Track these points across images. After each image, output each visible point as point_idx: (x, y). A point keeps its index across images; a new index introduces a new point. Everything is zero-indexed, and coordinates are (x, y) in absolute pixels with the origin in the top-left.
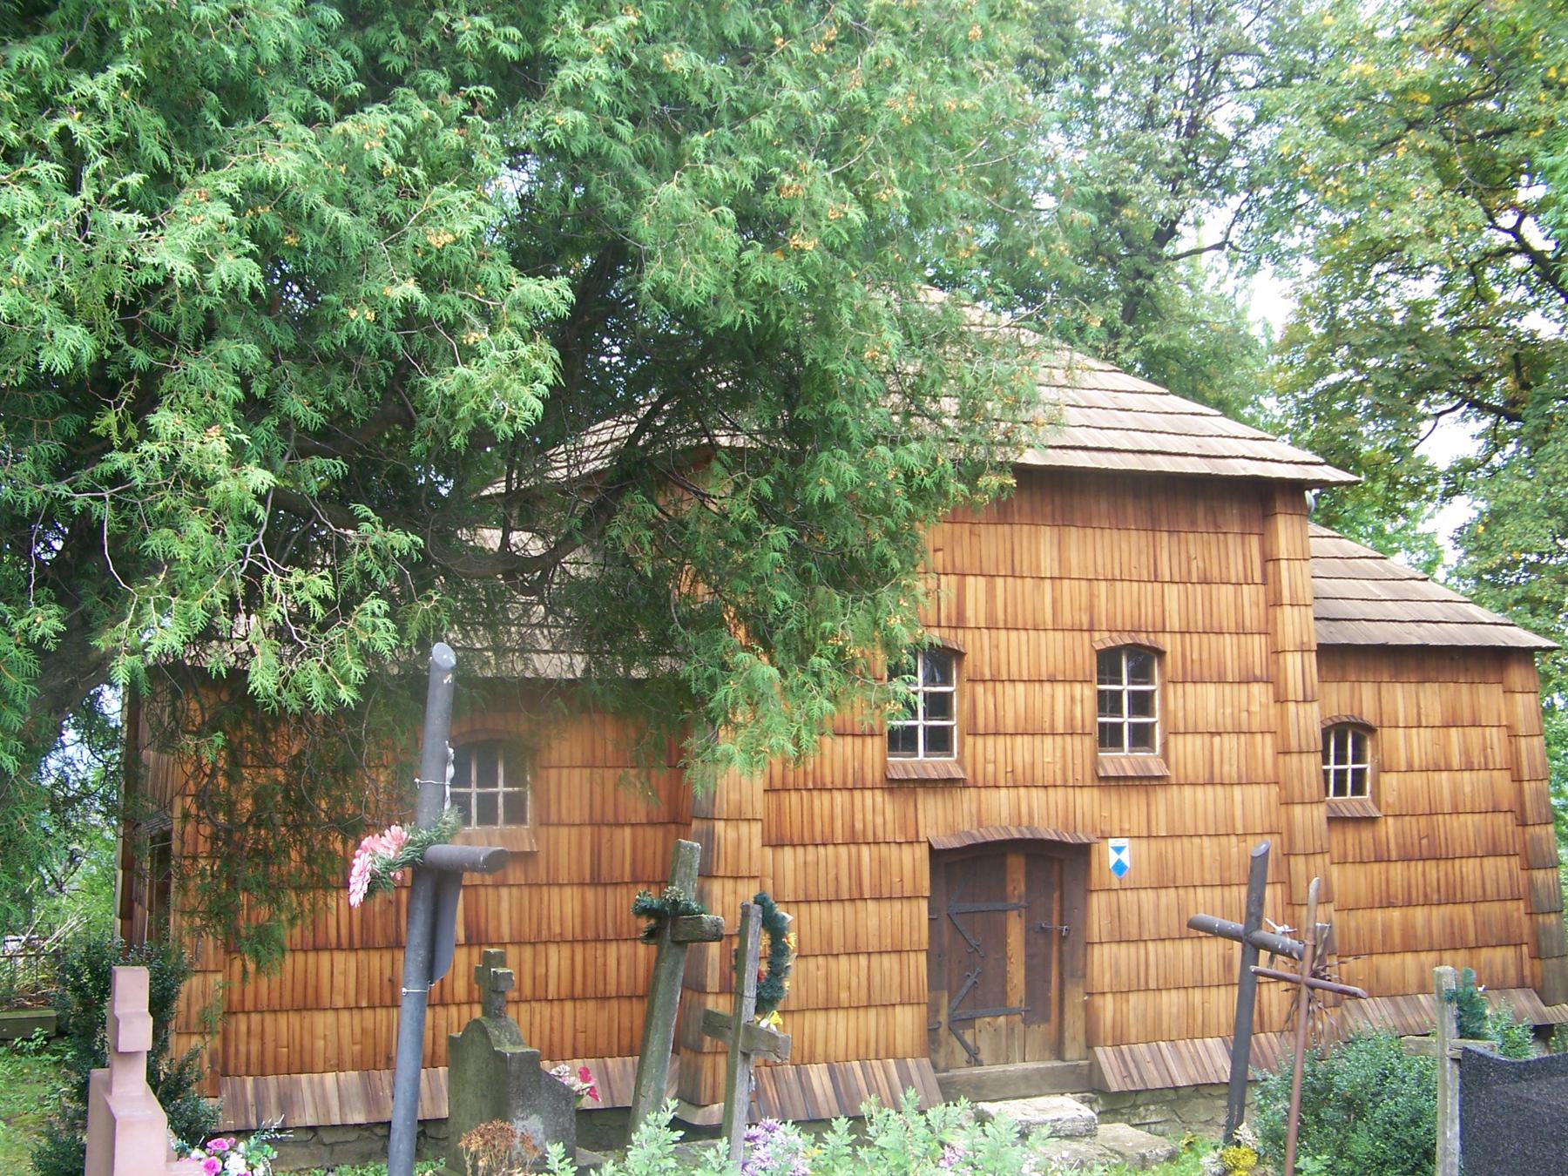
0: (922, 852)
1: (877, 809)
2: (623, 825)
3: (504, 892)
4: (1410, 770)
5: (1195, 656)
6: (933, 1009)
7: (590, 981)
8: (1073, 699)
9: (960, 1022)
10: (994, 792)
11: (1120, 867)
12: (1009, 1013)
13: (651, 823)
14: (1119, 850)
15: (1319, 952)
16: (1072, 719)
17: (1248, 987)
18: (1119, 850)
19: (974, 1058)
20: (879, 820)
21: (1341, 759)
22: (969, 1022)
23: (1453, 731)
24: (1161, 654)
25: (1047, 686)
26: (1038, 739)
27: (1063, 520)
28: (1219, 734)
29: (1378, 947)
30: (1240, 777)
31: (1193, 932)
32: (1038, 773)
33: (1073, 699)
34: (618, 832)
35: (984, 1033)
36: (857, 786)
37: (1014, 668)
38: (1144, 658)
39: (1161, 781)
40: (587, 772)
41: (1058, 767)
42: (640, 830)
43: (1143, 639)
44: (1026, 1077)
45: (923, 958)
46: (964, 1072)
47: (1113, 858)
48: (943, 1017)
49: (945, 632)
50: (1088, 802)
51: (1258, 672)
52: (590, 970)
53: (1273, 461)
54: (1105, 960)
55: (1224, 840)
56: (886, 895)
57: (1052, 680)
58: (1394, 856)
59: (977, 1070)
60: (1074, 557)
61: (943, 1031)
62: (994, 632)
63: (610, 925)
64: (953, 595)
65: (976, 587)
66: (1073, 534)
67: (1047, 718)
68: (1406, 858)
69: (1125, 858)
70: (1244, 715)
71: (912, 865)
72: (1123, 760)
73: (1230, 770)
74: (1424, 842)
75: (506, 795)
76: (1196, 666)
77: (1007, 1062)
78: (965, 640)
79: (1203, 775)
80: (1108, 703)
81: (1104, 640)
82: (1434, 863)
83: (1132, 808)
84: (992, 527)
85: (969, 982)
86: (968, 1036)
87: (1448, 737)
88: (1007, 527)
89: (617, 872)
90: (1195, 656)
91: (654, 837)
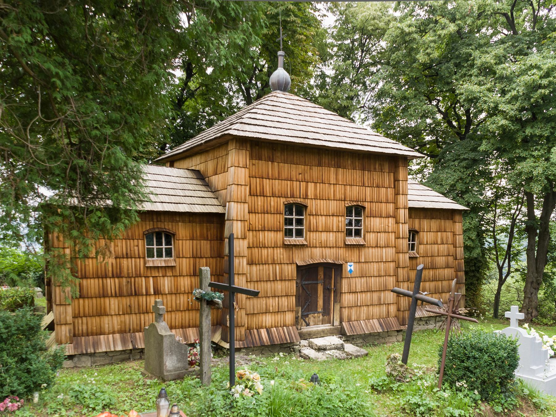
1: (280, 254)
3: (166, 278)
4: (427, 244)
5: (374, 209)
11: (351, 271)
12: (319, 313)
13: (211, 257)
14: (351, 266)
16: (339, 227)
18: (351, 266)
20: (282, 257)
26: (328, 233)
34: (201, 260)
40: (191, 241)
42: (208, 259)
45: (294, 298)
47: (349, 268)
48: (300, 314)
49: (302, 200)
50: (342, 252)
54: (347, 299)
55: (380, 263)
57: (333, 215)
60: (340, 177)
69: (352, 268)
71: (290, 270)
73: (382, 243)
75: (165, 248)
78: (308, 203)
81: (348, 204)
85: (307, 304)
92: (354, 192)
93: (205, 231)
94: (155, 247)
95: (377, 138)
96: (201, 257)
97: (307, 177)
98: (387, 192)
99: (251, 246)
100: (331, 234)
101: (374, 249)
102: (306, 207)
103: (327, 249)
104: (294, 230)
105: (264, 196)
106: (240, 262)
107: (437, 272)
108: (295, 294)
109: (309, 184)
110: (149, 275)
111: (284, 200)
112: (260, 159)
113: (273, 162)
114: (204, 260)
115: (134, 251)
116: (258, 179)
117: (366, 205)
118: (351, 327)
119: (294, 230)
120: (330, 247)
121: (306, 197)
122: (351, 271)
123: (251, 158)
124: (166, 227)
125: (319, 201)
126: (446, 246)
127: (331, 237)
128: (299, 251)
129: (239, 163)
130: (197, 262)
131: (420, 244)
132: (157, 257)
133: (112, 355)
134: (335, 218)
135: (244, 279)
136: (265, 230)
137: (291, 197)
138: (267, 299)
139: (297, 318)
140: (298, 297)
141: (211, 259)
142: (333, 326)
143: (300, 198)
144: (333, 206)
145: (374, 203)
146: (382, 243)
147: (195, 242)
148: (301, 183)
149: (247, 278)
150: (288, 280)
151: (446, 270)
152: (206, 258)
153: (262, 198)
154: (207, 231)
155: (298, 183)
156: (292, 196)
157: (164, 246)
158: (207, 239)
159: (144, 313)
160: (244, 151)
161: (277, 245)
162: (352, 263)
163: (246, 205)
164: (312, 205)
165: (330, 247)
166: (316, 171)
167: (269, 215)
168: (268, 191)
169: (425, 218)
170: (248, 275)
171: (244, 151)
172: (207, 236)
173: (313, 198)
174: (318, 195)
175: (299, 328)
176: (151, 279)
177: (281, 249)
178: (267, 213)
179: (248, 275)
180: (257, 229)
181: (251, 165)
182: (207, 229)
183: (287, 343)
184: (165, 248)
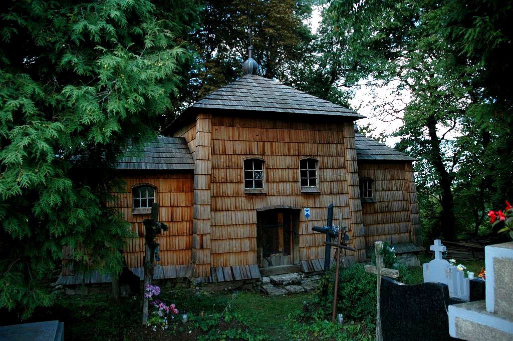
0: (255, 213)
1: (243, 202)
2: (179, 207)
4: (383, 190)
5: (326, 162)
6: (258, 253)
7: (171, 246)
8: (294, 173)
9: (266, 255)
10: (273, 197)
11: (307, 216)
12: (280, 252)
13: (187, 206)
14: (307, 211)
15: (343, 236)
16: (294, 177)
17: (328, 246)
18: (307, 211)
19: (270, 264)
20: (243, 205)
21: (365, 188)
22: (269, 256)
23: (393, 181)
24: (317, 161)
25: (287, 170)
26: (285, 184)
27: (290, 127)
28: (333, 181)
29: (387, 233)
30: (338, 192)
31: (315, 232)
32: (285, 192)
33: (294, 173)
34: (178, 209)
35: (274, 257)
36: (237, 196)
37: (278, 165)
38: (259, 164)
39: (265, 195)
40: (170, 193)
41: (290, 190)
42: (183, 208)
43: (312, 158)
44: (284, 269)
45: (255, 240)
46: (268, 268)
47: (306, 213)
49: (260, 156)
50: (300, 200)
51: (342, 166)
52: (172, 243)
53: (311, 110)
56: (245, 223)
58: (379, 211)
59: (271, 268)
60: (293, 137)
61: (262, 258)
62: (273, 156)
63: (176, 232)
64: (262, 146)
65: (268, 145)
66: (293, 131)
67: (287, 177)
68: (382, 212)
69: (309, 213)
70: (339, 176)
72: (254, 190)
73: (335, 190)
74: (387, 208)
75: (148, 199)
76: (326, 164)
77: (279, 265)
78: (265, 158)
79: (329, 192)
80: (303, 174)
81: (303, 158)
82: (389, 213)
83: (311, 202)
84: (272, 130)
86: (269, 258)
87: (392, 183)
88: (276, 130)
89: (178, 219)
90: (326, 162)
91: (187, 210)
92: (308, 149)
93: (181, 184)
94: (140, 198)
95: (328, 105)
96: (177, 207)
97: (264, 138)
98: (337, 147)
99: (215, 195)
100: (288, 184)
101: (328, 196)
102: (263, 162)
103: (284, 196)
104: (254, 182)
105: (226, 155)
106: (204, 210)
107: (394, 215)
108: (326, 218)
109: (266, 143)
110: (135, 221)
111: (244, 157)
112: (222, 125)
113: (233, 126)
114: (180, 208)
115: (124, 202)
116: (220, 141)
117: (318, 158)
118: (309, 265)
119: (254, 182)
120: (287, 195)
121: (264, 154)
122: (307, 216)
123: (213, 124)
124: (150, 183)
125: (275, 157)
126: (401, 192)
127: (288, 187)
128: (260, 198)
129: (229, 138)
130: (174, 210)
131: (376, 191)
132: (142, 207)
133: (105, 286)
134: (291, 171)
135: (209, 224)
136: (227, 182)
137: (249, 155)
138: (231, 241)
139: (259, 257)
140: (259, 238)
141: (186, 208)
142: (293, 264)
143: (258, 155)
144: (289, 161)
145: (326, 158)
146: (335, 190)
147: (172, 194)
148: (266, 143)
149: (212, 223)
150: (250, 224)
151: (402, 213)
152: (182, 207)
153: (225, 156)
154: (183, 185)
155: (256, 143)
156: (251, 154)
157: (140, 198)
158: (183, 192)
159: (130, 252)
160: (207, 120)
161: (238, 194)
162: (309, 209)
163: (209, 162)
164: (270, 161)
165: (287, 195)
166: (271, 133)
167: (231, 170)
168: (229, 151)
169: (379, 168)
170: (213, 220)
171: (207, 120)
172: (183, 189)
173: (269, 154)
174: (274, 152)
175: (262, 266)
176: (137, 225)
177: (301, 197)
178: (229, 168)
179: (213, 220)
180: (220, 181)
181: (214, 130)
182: (183, 183)
183: (249, 279)
184: (148, 199)
